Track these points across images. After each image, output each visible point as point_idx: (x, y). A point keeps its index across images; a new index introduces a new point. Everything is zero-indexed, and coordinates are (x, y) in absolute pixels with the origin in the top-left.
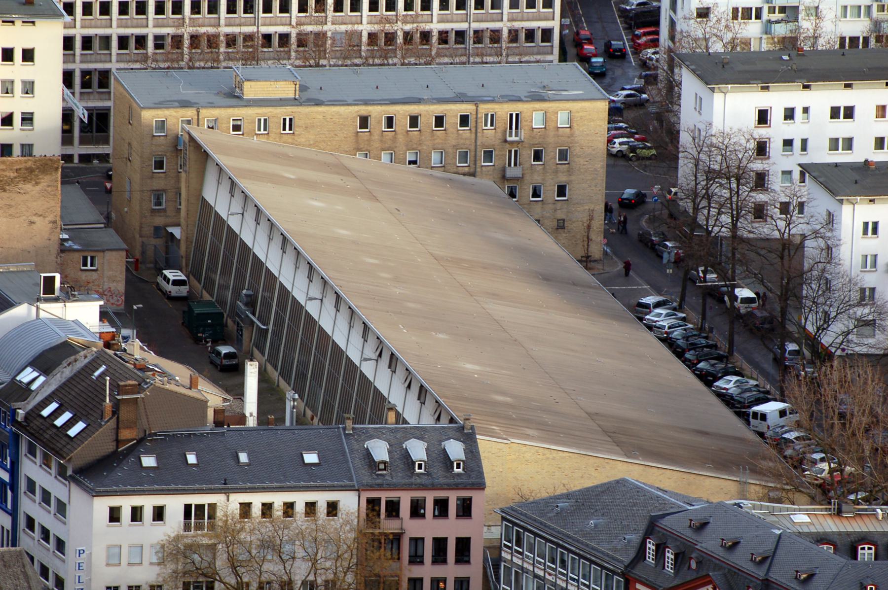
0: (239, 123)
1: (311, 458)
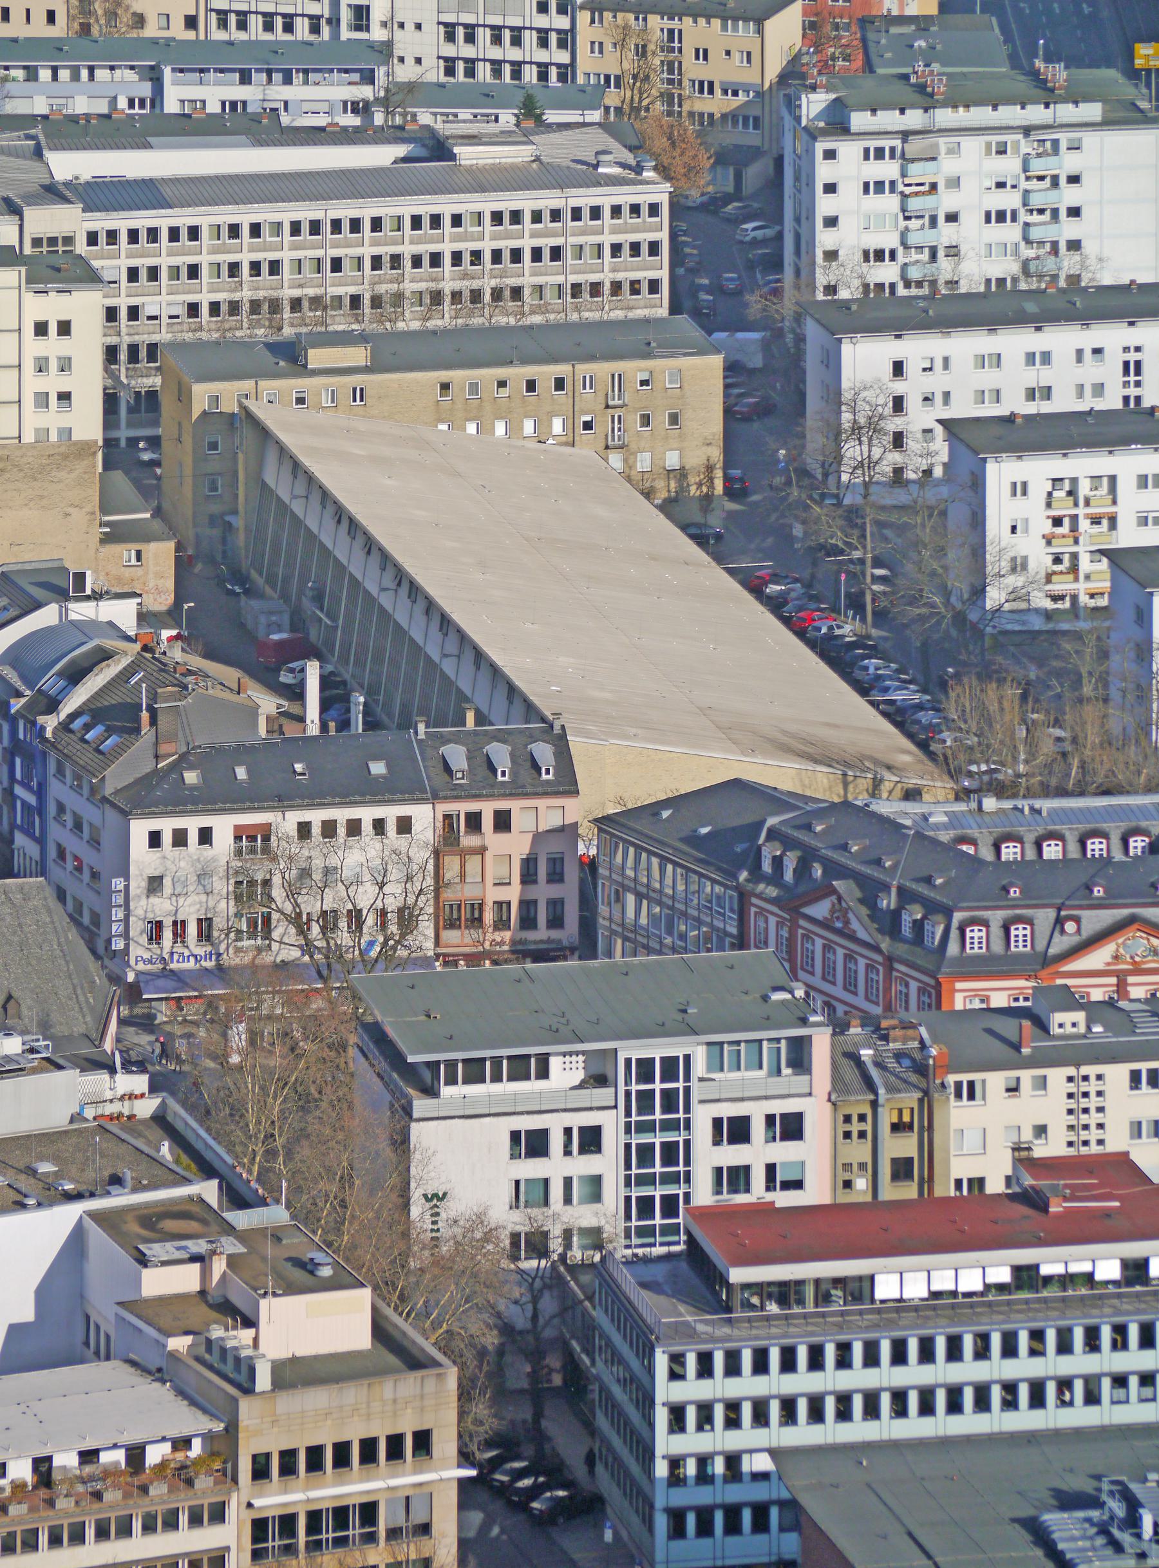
0: (301, 395)
1: (378, 768)
